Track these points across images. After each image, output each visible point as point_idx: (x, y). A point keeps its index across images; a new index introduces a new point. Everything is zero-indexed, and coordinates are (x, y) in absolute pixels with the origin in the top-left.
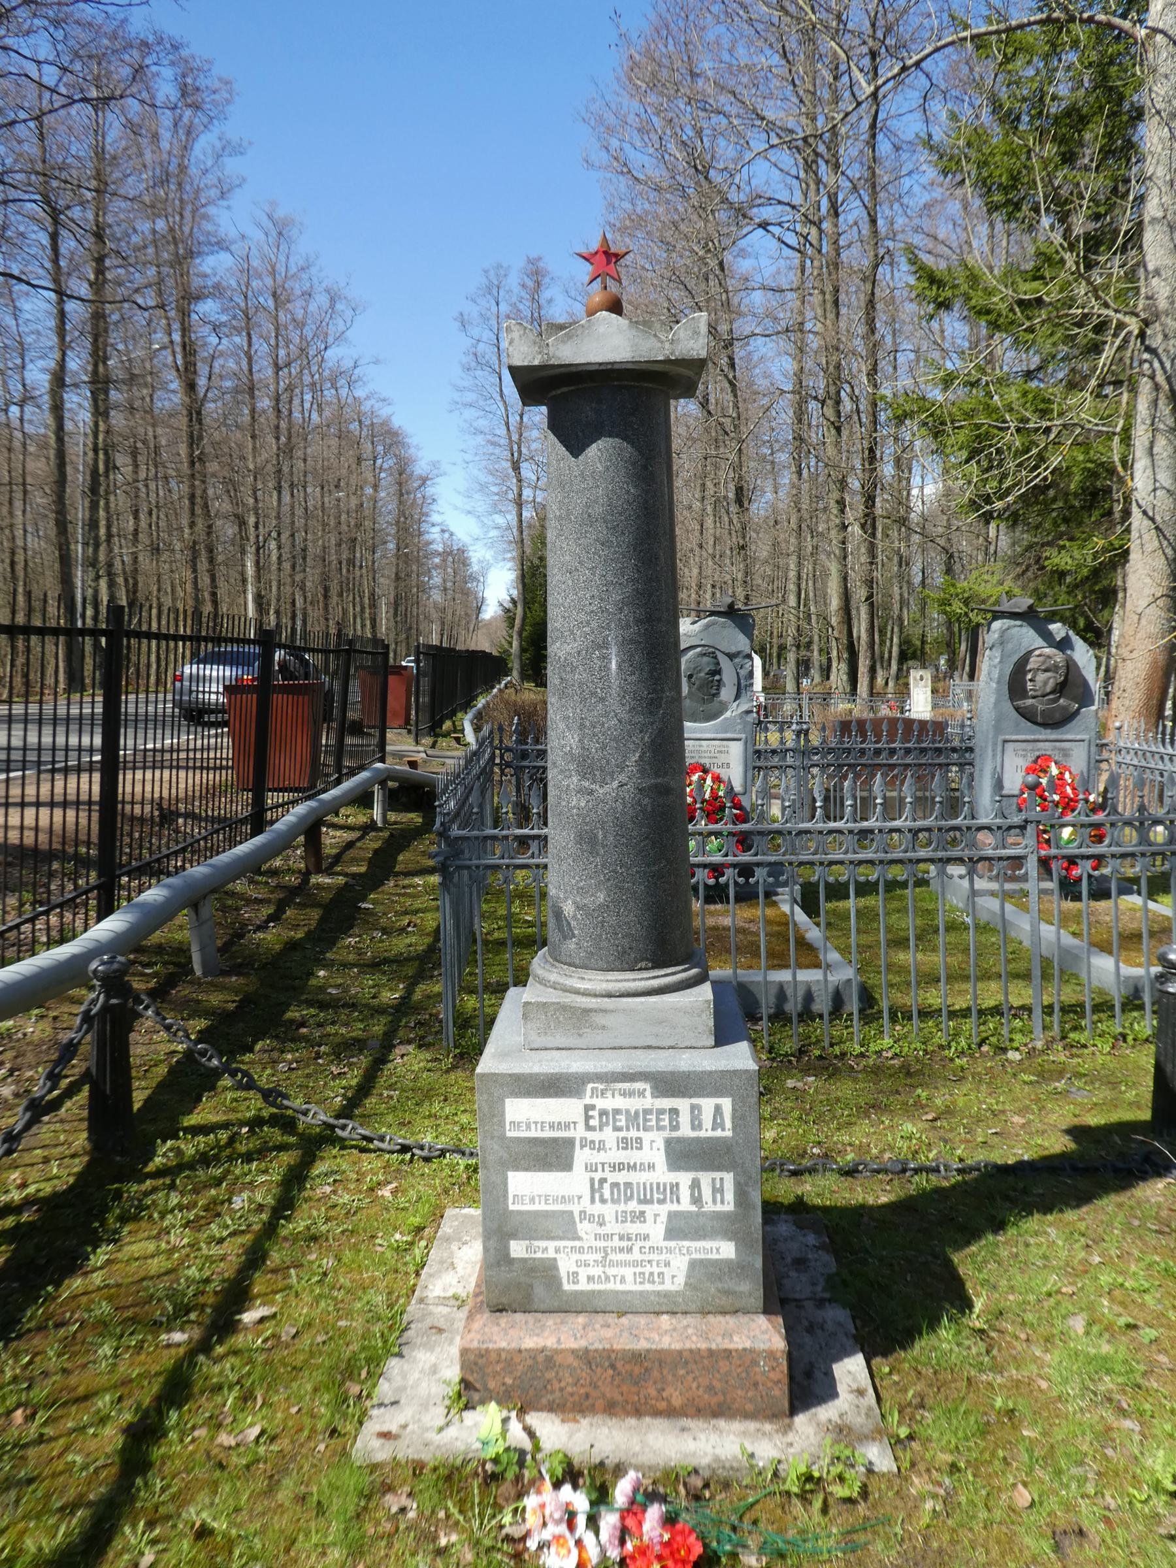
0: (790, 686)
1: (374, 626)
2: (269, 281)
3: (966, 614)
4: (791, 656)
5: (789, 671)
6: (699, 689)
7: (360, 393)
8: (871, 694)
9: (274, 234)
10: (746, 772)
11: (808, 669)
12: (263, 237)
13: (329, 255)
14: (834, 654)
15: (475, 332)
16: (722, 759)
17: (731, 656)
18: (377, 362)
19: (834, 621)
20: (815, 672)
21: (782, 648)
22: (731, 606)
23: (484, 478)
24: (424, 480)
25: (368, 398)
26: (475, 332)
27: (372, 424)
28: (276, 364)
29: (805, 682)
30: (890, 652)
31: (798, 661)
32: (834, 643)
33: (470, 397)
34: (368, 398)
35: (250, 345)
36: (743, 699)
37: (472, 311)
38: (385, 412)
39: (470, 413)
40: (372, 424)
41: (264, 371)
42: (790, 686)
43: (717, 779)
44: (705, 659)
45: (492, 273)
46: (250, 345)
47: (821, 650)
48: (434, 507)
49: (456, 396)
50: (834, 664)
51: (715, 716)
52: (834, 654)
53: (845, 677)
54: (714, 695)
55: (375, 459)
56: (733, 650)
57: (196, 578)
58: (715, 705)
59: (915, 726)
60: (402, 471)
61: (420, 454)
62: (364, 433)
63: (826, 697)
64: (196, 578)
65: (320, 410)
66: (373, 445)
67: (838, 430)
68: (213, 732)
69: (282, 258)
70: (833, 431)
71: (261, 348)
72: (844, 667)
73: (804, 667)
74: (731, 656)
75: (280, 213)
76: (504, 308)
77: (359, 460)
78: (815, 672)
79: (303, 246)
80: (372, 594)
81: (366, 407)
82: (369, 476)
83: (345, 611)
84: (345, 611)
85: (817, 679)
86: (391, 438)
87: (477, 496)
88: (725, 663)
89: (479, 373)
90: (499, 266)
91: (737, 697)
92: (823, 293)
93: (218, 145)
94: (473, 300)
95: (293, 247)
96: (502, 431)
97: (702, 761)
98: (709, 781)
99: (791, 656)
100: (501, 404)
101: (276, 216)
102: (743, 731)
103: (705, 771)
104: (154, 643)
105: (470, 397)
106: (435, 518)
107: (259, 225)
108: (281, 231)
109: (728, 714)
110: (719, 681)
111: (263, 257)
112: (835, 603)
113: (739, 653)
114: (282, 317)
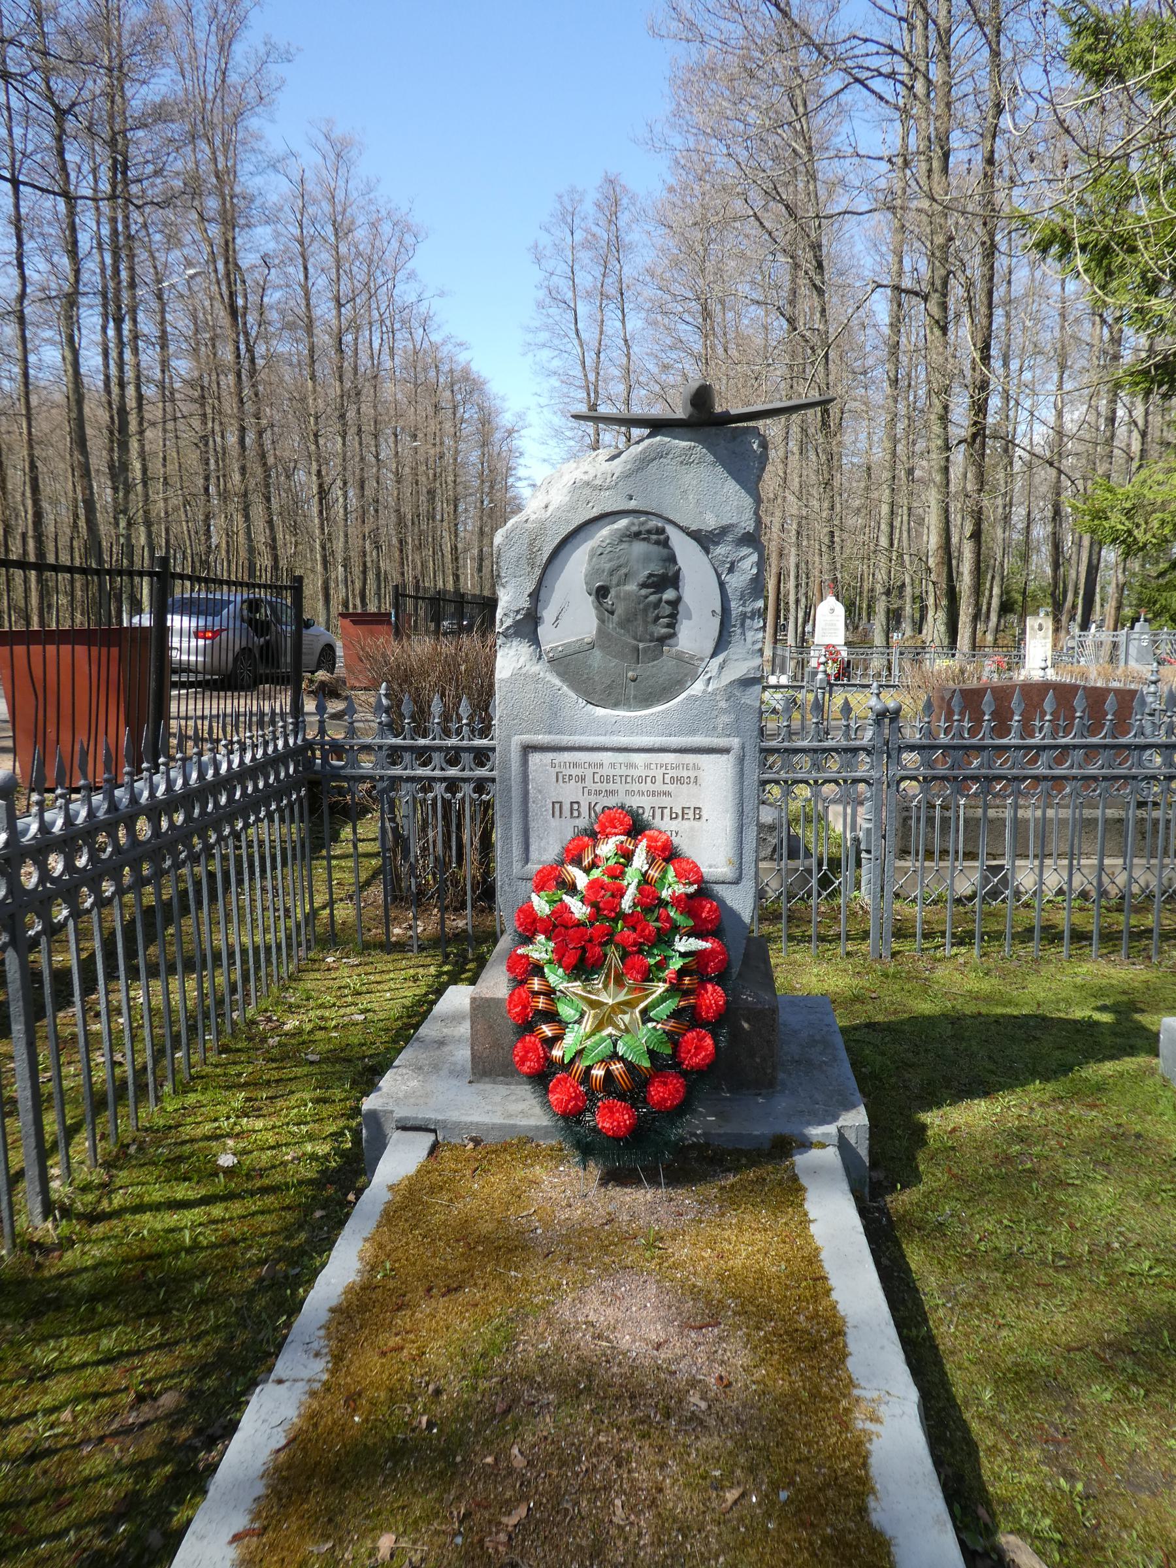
0: (878, 639)
1: (457, 577)
2: (326, 207)
3: (1130, 532)
4: (881, 607)
5: (879, 621)
6: (625, 623)
7: (436, 337)
8: (974, 647)
9: (333, 156)
10: (740, 829)
11: (899, 622)
12: (320, 160)
13: (392, 177)
14: (931, 601)
15: (550, 265)
16: (682, 797)
17: (704, 540)
18: (441, 294)
19: (932, 562)
20: (907, 626)
21: (872, 601)
22: (702, 398)
23: (558, 421)
24: (510, 432)
25: (444, 343)
26: (550, 265)
27: (451, 371)
28: (337, 300)
29: (896, 636)
30: (989, 604)
31: (888, 611)
32: (931, 588)
33: (544, 336)
34: (444, 343)
35: (306, 277)
36: (736, 650)
37: (545, 240)
38: (462, 357)
39: (545, 354)
40: (451, 371)
41: (324, 309)
42: (878, 639)
43: (667, 853)
44: (639, 548)
45: (565, 199)
46: (306, 277)
47: (914, 599)
48: (521, 461)
49: (529, 337)
50: (931, 613)
51: (648, 698)
52: (931, 601)
53: (943, 628)
54: (662, 640)
55: (455, 408)
56: (710, 522)
57: (248, 527)
58: (666, 665)
59: (1110, 703)
60: (486, 421)
61: (507, 405)
62: (441, 380)
63: (918, 653)
64: (248, 527)
65: (392, 355)
66: (448, 396)
67: (944, 330)
68: (183, 692)
69: (341, 183)
70: (937, 332)
71: (320, 282)
72: (942, 616)
73: (894, 617)
74: (704, 540)
75: (337, 133)
76: (579, 236)
77: (437, 407)
78: (907, 626)
79: (364, 167)
80: (455, 548)
81: (444, 352)
82: (448, 425)
83: (424, 565)
84: (424, 565)
85: (909, 633)
86: (467, 384)
87: (553, 442)
88: (686, 552)
89: (553, 311)
90: (573, 190)
91: (722, 643)
92: (929, 160)
93: (262, 50)
94: (547, 230)
95: (352, 170)
96: (577, 372)
97: (634, 802)
98: (640, 860)
99: (881, 607)
100: (576, 342)
101: (333, 136)
102: (735, 729)
103: (636, 827)
104: (33, 574)
105: (544, 336)
106: (521, 472)
107: (315, 147)
108: (340, 153)
109: (697, 687)
110: (675, 603)
111: (320, 182)
112: (933, 541)
113: (724, 531)
114: (343, 249)
